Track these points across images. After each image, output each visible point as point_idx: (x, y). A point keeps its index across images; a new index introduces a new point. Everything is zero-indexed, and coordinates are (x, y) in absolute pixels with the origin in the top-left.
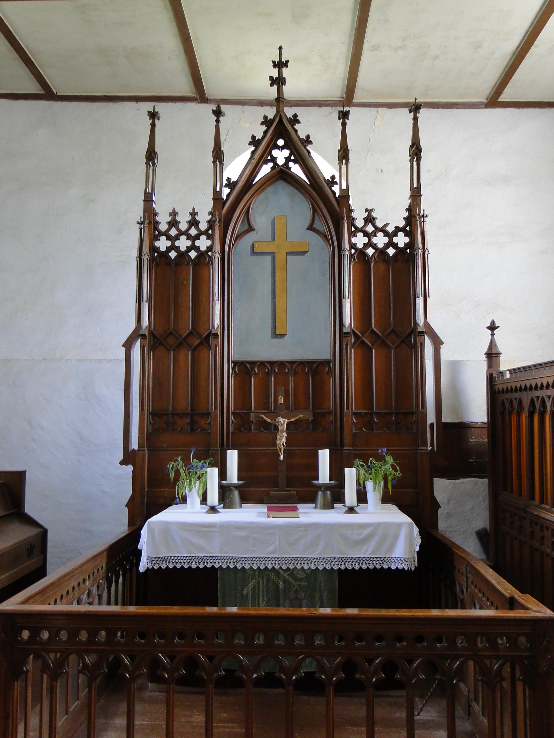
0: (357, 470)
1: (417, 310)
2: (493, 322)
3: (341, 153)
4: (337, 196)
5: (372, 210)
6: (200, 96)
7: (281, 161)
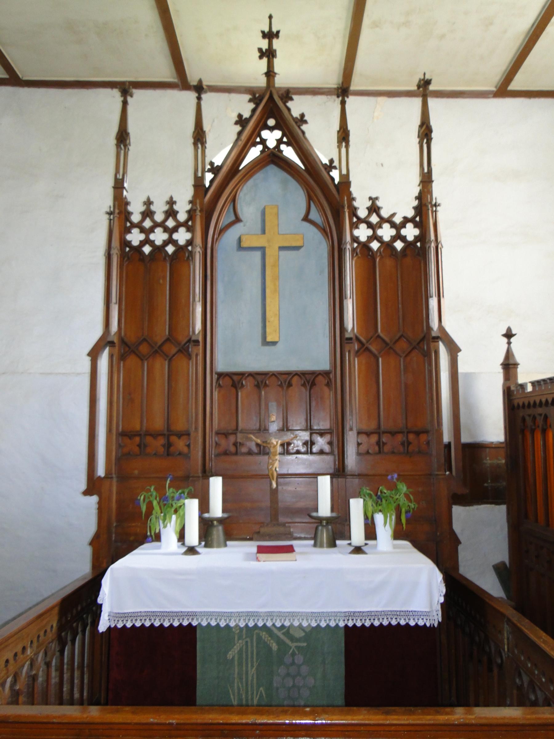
0: (364, 500)
1: (431, 312)
2: (509, 329)
3: (340, 134)
4: (336, 182)
5: (377, 198)
6: (182, 82)
7: (271, 144)
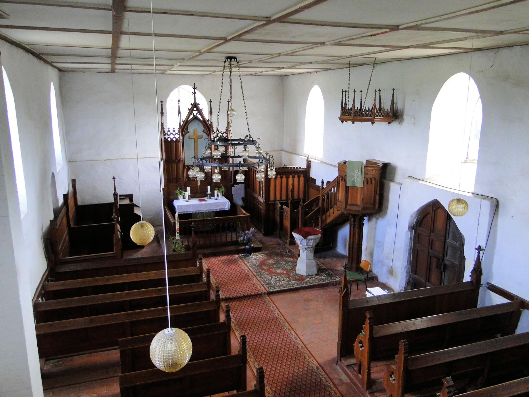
7: (195, 114)
